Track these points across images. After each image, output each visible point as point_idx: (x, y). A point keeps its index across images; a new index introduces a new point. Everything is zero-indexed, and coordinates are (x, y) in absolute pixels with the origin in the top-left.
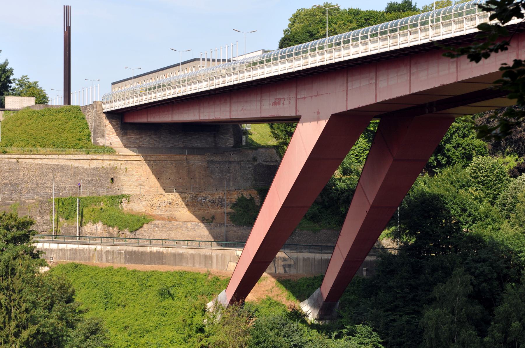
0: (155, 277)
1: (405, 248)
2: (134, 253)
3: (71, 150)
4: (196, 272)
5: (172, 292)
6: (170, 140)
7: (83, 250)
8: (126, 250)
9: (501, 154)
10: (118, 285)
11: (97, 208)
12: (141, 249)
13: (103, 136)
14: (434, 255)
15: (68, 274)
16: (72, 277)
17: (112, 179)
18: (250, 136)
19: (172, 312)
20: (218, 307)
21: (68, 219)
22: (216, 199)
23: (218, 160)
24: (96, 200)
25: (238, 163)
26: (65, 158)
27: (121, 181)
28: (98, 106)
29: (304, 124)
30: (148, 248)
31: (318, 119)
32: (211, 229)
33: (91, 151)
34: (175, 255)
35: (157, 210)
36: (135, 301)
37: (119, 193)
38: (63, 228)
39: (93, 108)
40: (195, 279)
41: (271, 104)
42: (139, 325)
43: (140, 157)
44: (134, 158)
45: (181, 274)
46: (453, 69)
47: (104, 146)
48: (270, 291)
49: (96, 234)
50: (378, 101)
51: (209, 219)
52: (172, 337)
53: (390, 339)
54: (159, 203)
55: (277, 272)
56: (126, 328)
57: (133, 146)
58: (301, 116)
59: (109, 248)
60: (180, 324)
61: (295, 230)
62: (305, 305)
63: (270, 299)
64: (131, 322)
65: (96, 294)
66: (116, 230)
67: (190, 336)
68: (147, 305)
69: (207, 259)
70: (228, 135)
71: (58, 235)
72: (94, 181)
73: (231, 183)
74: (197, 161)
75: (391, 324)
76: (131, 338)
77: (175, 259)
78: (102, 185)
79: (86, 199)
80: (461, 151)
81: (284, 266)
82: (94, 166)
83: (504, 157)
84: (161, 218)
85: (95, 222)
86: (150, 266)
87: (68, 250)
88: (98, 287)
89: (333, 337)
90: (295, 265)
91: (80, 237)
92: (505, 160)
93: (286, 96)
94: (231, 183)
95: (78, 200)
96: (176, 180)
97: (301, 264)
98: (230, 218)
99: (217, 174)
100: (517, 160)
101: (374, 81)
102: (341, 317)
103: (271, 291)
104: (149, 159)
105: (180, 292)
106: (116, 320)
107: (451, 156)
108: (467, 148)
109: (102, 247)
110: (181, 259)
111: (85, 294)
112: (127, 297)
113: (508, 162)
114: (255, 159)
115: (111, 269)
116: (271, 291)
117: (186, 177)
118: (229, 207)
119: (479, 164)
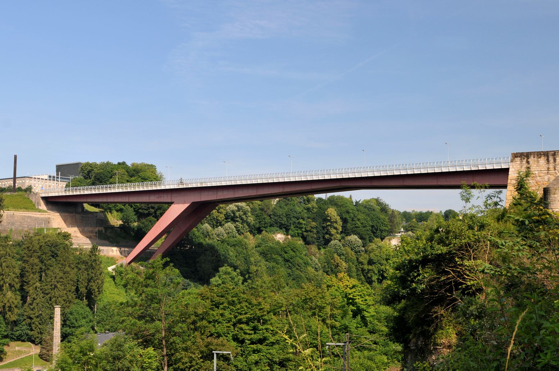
13: (41, 206)
114: (97, 216)
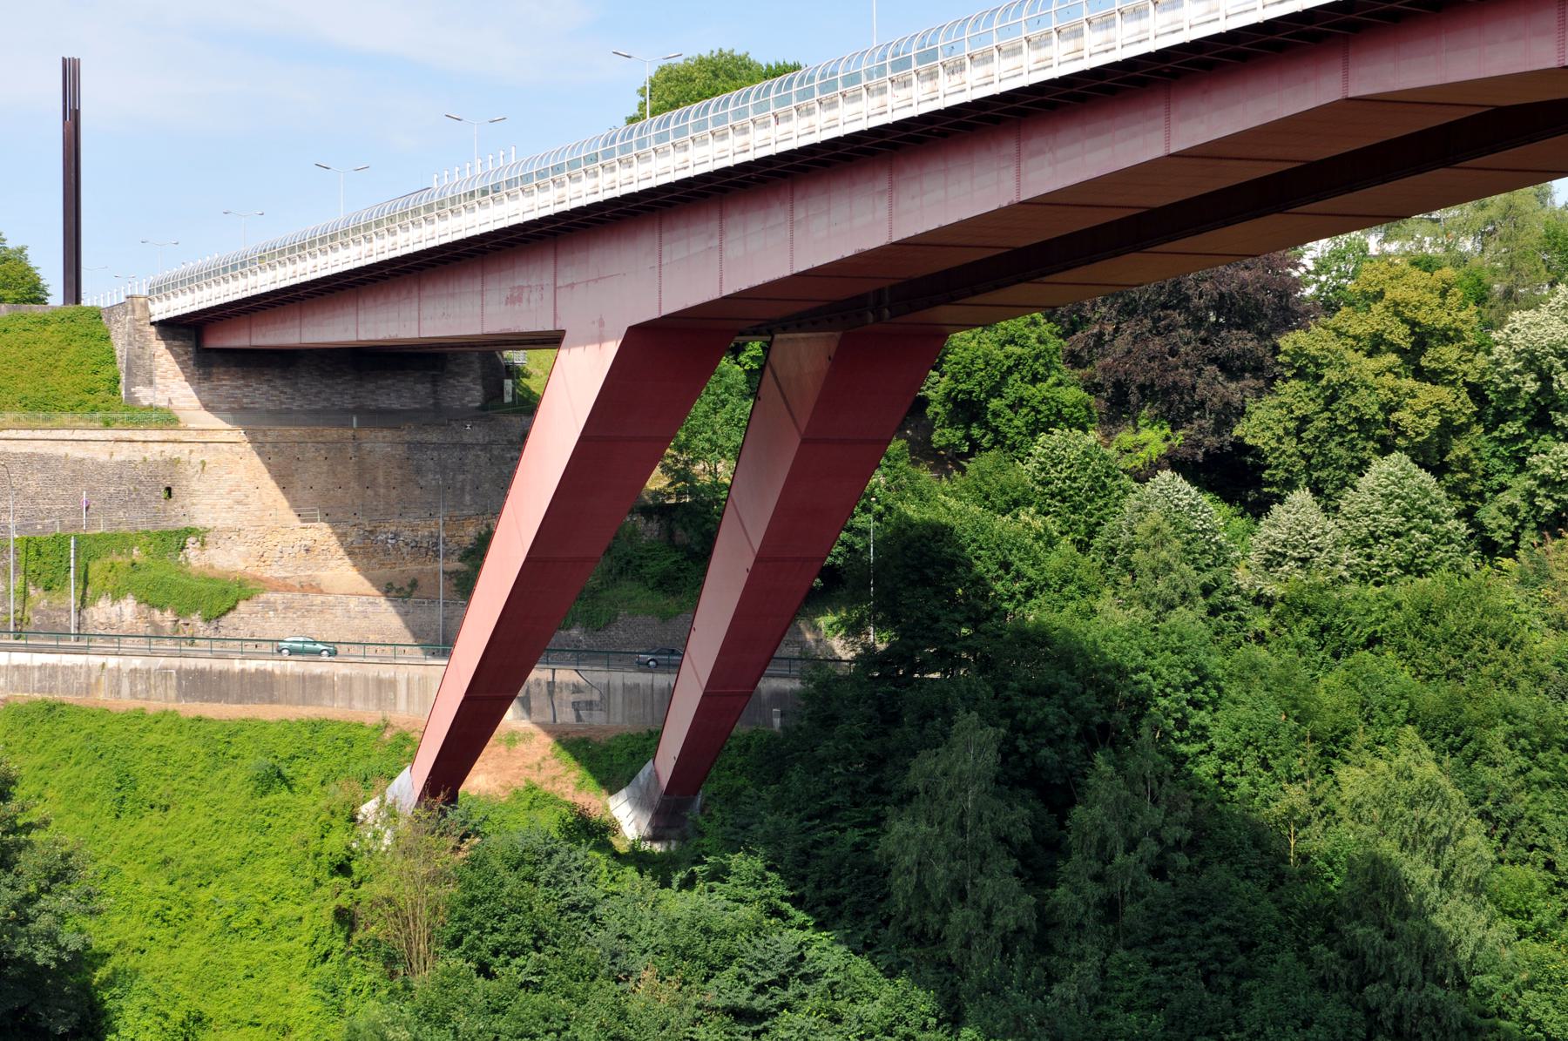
0: (248, 734)
1: (868, 658)
2: (201, 673)
3: (66, 418)
4: (355, 721)
5: (287, 772)
6: (320, 392)
7: (71, 668)
8: (181, 666)
9: (1130, 422)
10: (154, 756)
11: (122, 561)
12: (219, 665)
13: (151, 383)
14: (937, 675)
15: (30, 727)
16: (39, 735)
17: (169, 489)
18: (525, 381)
19: (284, 821)
20: (391, 813)
21: (50, 589)
22: (423, 537)
23: (435, 440)
24: (121, 542)
25: (485, 447)
26: (49, 437)
27: (191, 495)
28: (138, 308)
29: (573, 350)
30: (237, 661)
31: (601, 340)
32: (407, 613)
33: (116, 420)
34: (302, 679)
35: (275, 567)
36: (195, 795)
37: (184, 523)
38: (36, 612)
39: (126, 314)
40: (348, 738)
41: (504, 299)
42: (199, 857)
43: (239, 435)
44: (224, 436)
45: (316, 727)
46: (882, 210)
47: (151, 406)
48: (536, 767)
49: (118, 628)
50: (724, 294)
51: (402, 589)
52: (278, 885)
53: (808, 889)
54: (279, 547)
55: (558, 721)
56: (166, 862)
57: (227, 406)
58: (564, 331)
59: (137, 662)
60: (297, 853)
61: (617, 615)
62: (620, 801)
63: (535, 788)
64: (178, 848)
65: (97, 779)
66: (169, 616)
67: (317, 883)
68: (224, 805)
69: (384, 688)
70: (468, 379)
71: (24, 629)
72: (122, 494)
73: (468, 498)
74: (381, 444)
75: (815, 851)
76: (174, 889)
77: (304, 688)
78: (143, 504)
79: (96, 539)
80: (1027, 415)
81: (576, 706)
82: (123, 458)
83: (1137, 431)
84: (283, 586)
85: (116, 596)
86: (239, 707)
87: (34, 667)
88: (103, 762)
89: (675, 885)
90: (605, 702)
91: (79, 636)
92: (1139, 437)
93: (534, 281)
94: (468, 498)
95: (72, 541)
96: (328, 490)
97: (619, 699)
98: (456, 585)
99: (431, 476)
100: (1167, 438)
101: (716, 242)
102: (702, 834)
103: (540, 768)
104: (260, 438)
105: (309, 773)
106: (142, 843)
107: (1003, 428)
108: (1043, 408)
109: (121, 659)
110: (319, 687)
111: (69, 779)
112: (175, 786)
113: (1145, 444)
115: (141, 714)
116: (540, 768)
117: (352, 485)
118: (455, 557)
119: (1054, 449)
